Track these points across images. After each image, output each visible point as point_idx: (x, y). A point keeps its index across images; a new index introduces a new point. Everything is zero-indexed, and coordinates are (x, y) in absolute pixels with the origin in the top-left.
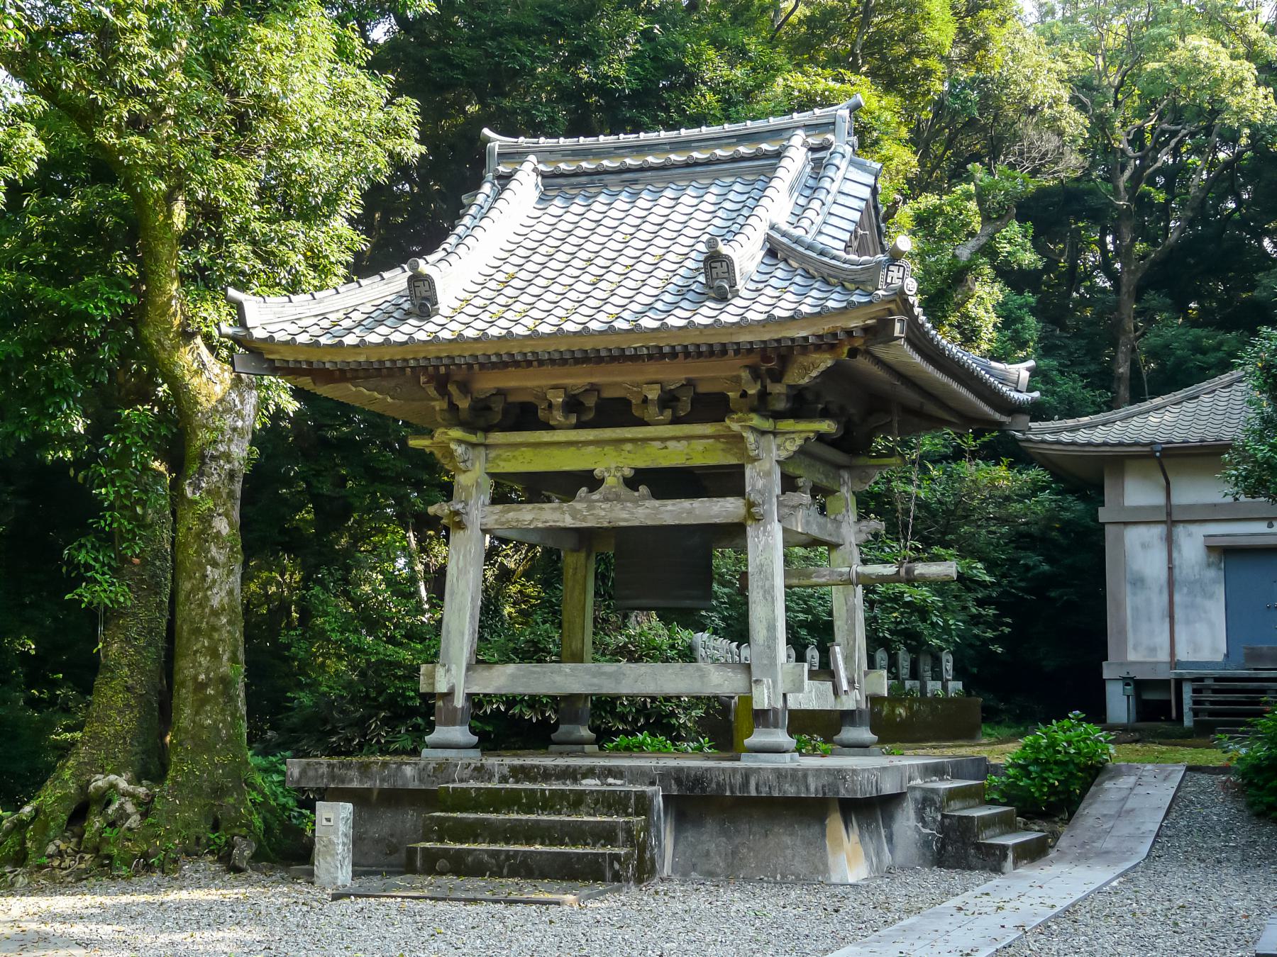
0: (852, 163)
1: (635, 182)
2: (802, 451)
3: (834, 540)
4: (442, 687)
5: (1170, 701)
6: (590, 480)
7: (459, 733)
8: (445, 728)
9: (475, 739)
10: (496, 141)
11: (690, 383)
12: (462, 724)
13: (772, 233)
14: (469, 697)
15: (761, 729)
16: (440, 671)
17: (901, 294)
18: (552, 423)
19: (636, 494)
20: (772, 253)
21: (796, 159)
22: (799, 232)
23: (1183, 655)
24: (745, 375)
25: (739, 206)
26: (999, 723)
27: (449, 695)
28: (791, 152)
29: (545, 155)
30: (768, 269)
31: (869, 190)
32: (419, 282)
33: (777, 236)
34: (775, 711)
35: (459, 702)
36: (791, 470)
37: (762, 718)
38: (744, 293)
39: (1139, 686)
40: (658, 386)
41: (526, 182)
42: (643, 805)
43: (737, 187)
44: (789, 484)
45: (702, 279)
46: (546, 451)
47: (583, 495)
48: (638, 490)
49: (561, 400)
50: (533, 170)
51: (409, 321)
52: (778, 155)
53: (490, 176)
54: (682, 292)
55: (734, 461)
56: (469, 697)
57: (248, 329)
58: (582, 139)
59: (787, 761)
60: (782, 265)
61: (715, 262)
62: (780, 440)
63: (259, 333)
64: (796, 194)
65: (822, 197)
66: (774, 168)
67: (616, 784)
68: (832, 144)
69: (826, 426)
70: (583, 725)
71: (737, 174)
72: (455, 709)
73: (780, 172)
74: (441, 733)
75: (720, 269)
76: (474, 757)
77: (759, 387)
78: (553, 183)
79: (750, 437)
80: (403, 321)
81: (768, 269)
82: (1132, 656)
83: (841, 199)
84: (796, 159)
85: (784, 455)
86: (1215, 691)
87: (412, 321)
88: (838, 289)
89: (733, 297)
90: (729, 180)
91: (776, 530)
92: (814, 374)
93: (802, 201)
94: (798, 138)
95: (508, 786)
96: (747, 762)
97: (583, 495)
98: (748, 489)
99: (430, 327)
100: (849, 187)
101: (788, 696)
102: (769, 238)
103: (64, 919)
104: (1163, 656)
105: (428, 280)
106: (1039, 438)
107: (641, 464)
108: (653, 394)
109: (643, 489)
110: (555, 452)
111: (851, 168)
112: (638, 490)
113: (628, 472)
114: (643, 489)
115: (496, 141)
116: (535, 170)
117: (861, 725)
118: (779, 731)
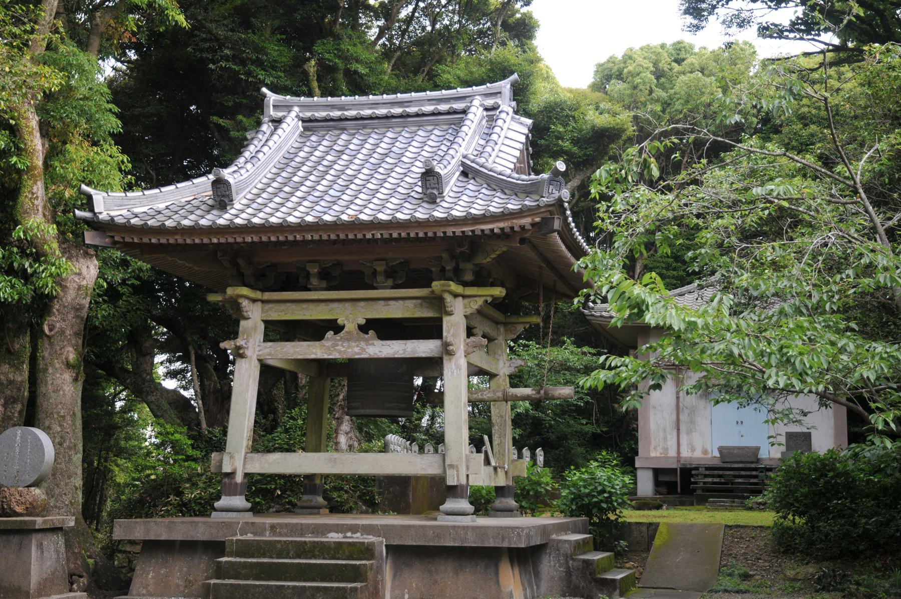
0: (513, 118)
1: (364, 127)
2: (479, 312)
3: (493, 371)
4: (227, 469)
5: (677, 482)
6: (336, 327)
7: (239, 501)
8: (228, 497)
9: (249, 505)
10: (272, 98)
11: (406, 263)
12: (241, 494)
13: (464, 160)
14: (246, 475)
15: (451, 499)
16: (226, 458)
17: (560, 201)
18: (309, 286)
19: (366, 336)
20: (464, 174)
21: (476, 113)
22: (482, 160)
23: (685, 453)
24: (445, 255)
25: (439, 144)
26: (335, 542)
27: (231, 475)
28: (473, 109)
29: (303, 107)
30: (462, 184)
31: (524, 137)
32: (220, 185)
33: (468, 162)
34: (461, 486)
35: (239, 478)
36: (472, 324)
37: (453, 491)
38: (447, 199)
39: (657, 472)
40: (384, 262)
41: (292, 124)
42: (366, 551)
43: (436, 132)
44: (470, 332)
45: (419, 190)
46: (305, 305)
47: (330, 336)
48: (368, 334)
49: (316, 270)
50: (296, 117)
51: (212, 212)
52: (464, 112)
53: (266, 119)
54: (407, 197)
55: (436, 315)
56: (246, 475)
57: (95, 214)
58: (329, 98)
59: (467, 521)
60: (472, 181)
61: (429, 176)
62: (466, 301)
63: (103, 216)
64: (477, 137)
65: (448, 159)
66: (462, 120)
67: (358, 537)
68: (499, 106)
69: (498, 292)
70: (319, 495)
71: (436, 124)
72: (236, 484)
73: (467, 122)
74: (225, 501)
75: (432, 181)
76: (249, 517)
77: (454, 264)
78: (310, 125)
79: (448, 298)
80: (208, 212)
81: (462, 184)
82: (653, 454)
83: (507, 142)
84: (476, 113)
85: (469, 311)
86: (706, 476)
87: (215, 212)
88: (513, 197)
89: (441, 201)
90: (430, 128)
91: (463, 362)
92: (493, 256)
93: (482, 142)
94: (477, 102)
95: (264, 539)
96: (443, 521)
97: (330, 336)
98: (444, 334)
99: (227, 216)
100: (511, 134)
101: (470, 476)
102: (463, 164)
103: (659, 517)
104: (672, 453)
105: (226, 184)
106: (598, 314)
107: (370, 316)
108: (380, 267)
109: (371, 333)
110: (311, 306)
111: (512, 123)
112: (368, 334)
113: (363, 322)
114: (371, 333)
115: (272, 98)
116: (297, 116)
117: (509, 497)
118: (463, 500)
